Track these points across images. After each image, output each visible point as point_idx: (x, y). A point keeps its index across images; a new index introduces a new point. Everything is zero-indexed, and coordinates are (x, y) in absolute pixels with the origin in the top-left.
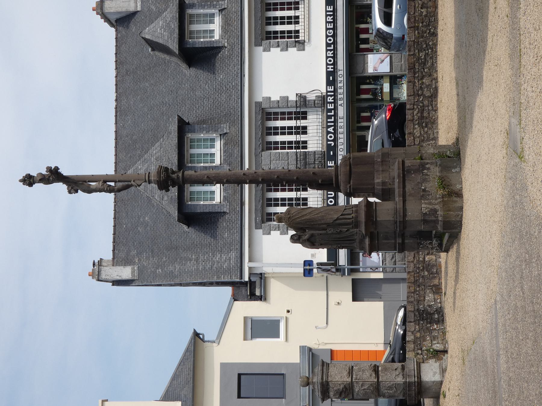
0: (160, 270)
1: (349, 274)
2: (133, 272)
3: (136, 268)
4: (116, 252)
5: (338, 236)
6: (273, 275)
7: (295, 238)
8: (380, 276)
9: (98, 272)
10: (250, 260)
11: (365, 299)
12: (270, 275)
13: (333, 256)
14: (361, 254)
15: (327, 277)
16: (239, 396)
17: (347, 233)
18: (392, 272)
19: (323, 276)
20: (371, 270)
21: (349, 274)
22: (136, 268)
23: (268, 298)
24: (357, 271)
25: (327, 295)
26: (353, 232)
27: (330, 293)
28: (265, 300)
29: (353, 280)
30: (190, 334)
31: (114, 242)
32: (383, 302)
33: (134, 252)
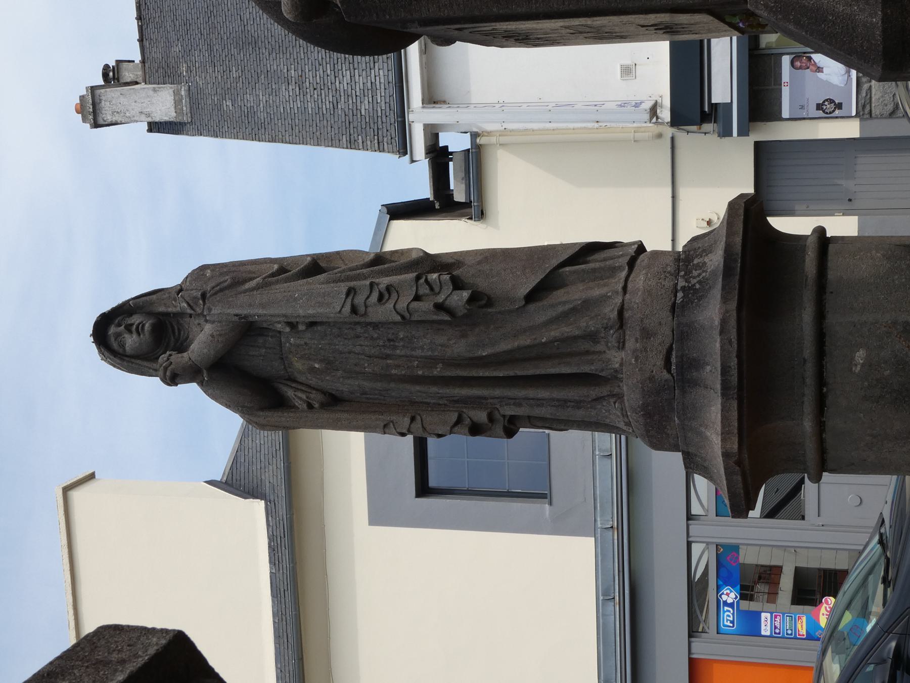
0: (229, 103)
1: (743, 132)
2: (177, 103)
3: (183, 93)
4: (147, 44)
5: (459, 347)
6: (503, 140)
7: (131, 341)
8: (850, 129)
9: (94, 104)
10: (431, 99)
11: (798, 207)
12: (493, 140)
13: (689, 70)
14: (786, 60)
15: (673, 139)
16: (423, 489)
17: (540, 313)
18: (892, 114)
19: (660, 136)
20: (820, 113)
21: (743, 132)
22: (183, 93)
23: (490, 210)
24: (774, 115)
25: (674, 197)
26: (587, 305)
27: (682, 192)
28: (481, 215)
29: (759, 147)
30: (91, 472)
31: (139, 18)
32: (857, 217)
33: (177, 49)
